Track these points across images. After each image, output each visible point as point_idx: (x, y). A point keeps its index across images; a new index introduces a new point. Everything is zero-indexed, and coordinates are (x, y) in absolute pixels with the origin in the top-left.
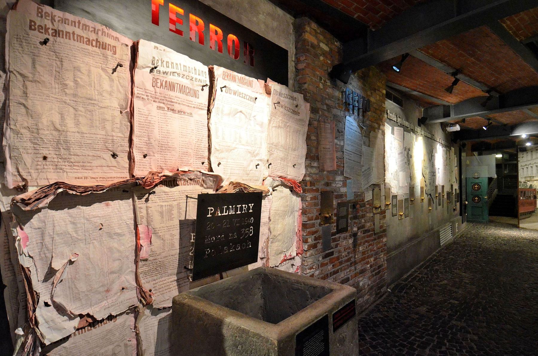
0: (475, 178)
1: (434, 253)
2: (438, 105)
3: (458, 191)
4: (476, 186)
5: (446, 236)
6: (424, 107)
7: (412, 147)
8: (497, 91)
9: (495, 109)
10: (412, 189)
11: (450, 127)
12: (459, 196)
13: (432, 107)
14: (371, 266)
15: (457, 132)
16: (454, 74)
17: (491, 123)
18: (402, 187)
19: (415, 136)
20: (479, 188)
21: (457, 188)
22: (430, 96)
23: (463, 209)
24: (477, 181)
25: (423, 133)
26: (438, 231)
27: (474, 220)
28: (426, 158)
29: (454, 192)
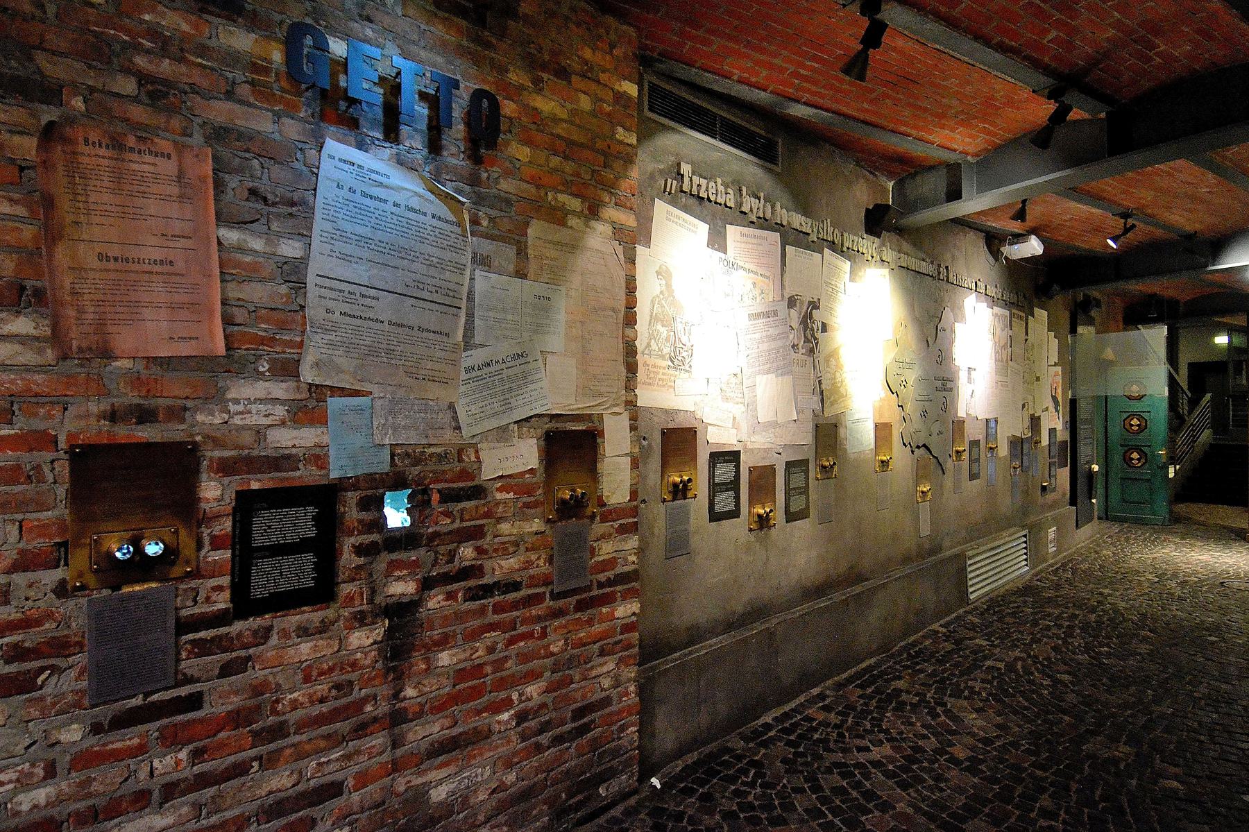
0: (1130, 398)
1: (936, 626)
2: (931, 168)
3: (1063, 435)
4: (1135, 422)
5: (999, 568)
6: (890, 175)
7: (831, 297)
8: (1092, 92)
9: (1097, 159)
10: (828, 433)
11: (1011, 244)
12: (1069, 451)
13: (916, 173)
14: (521, 717)
15: (1033, 260)
16: (1053, 95)
17: (1133, 226)
18: (774, 424)
19: (846, 265)
20: (1142, 428)
21: (1059, 426)
22: (863, 122)
23: (1082, 486)
24: (1136, 407)
25: (888, 255)
26: (960, 559)
27: (1126, 514)
28: (910, 336)
29: (1045, 441)
